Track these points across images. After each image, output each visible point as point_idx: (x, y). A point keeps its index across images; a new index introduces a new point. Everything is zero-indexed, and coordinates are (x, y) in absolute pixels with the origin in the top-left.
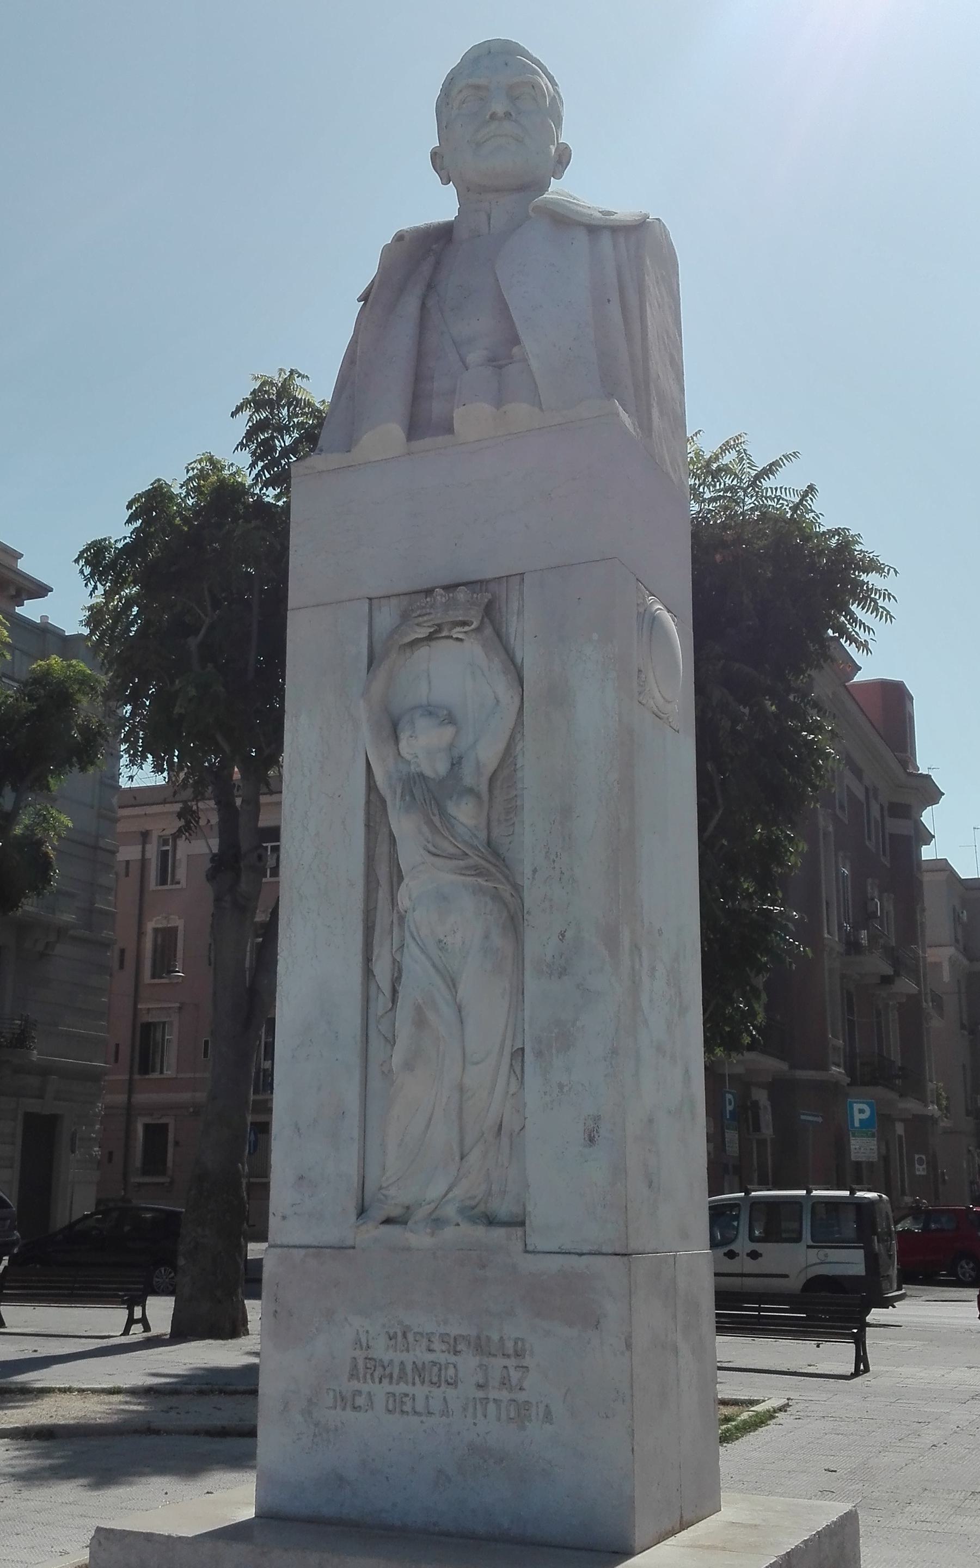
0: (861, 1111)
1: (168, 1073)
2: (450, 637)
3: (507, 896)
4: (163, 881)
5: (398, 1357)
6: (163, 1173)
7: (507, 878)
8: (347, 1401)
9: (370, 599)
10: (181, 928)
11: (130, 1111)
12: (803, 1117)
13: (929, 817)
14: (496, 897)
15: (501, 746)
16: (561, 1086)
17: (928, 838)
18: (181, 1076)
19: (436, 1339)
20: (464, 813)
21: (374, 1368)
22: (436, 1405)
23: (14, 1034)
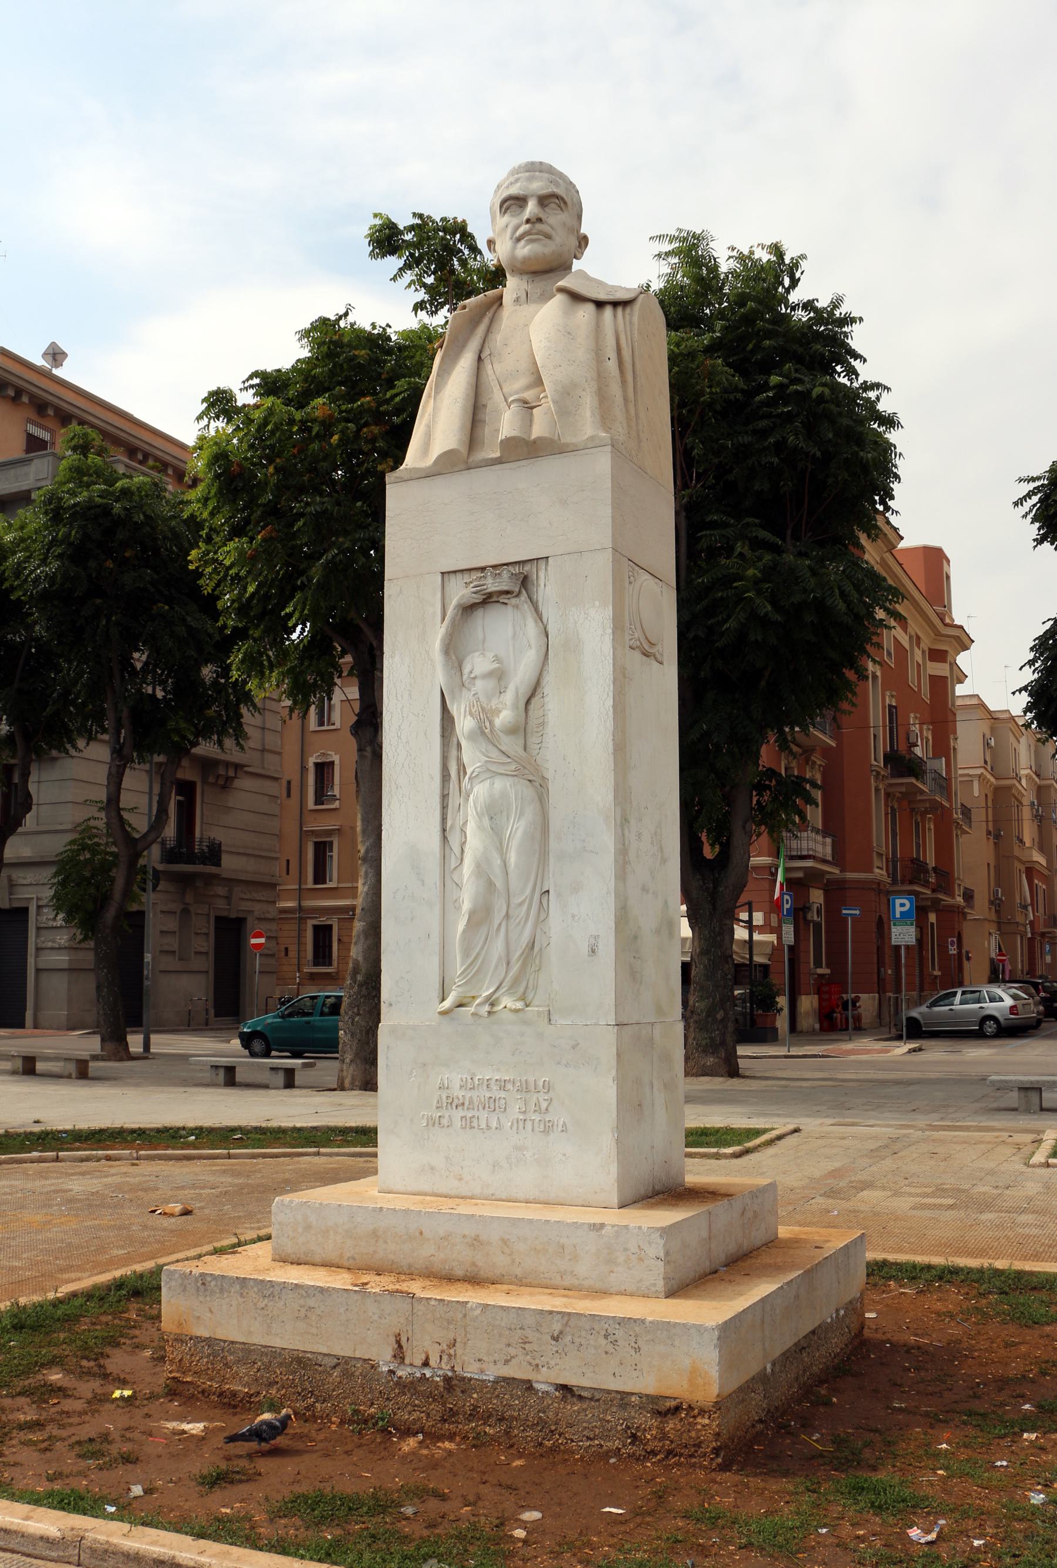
0: (903, 905)
10: (337, 762)
12: (844, 912)
13: (963, 660)
16: (573, 916)
17: (962, 678)
18: (341, 885)
19: (492, 1082)
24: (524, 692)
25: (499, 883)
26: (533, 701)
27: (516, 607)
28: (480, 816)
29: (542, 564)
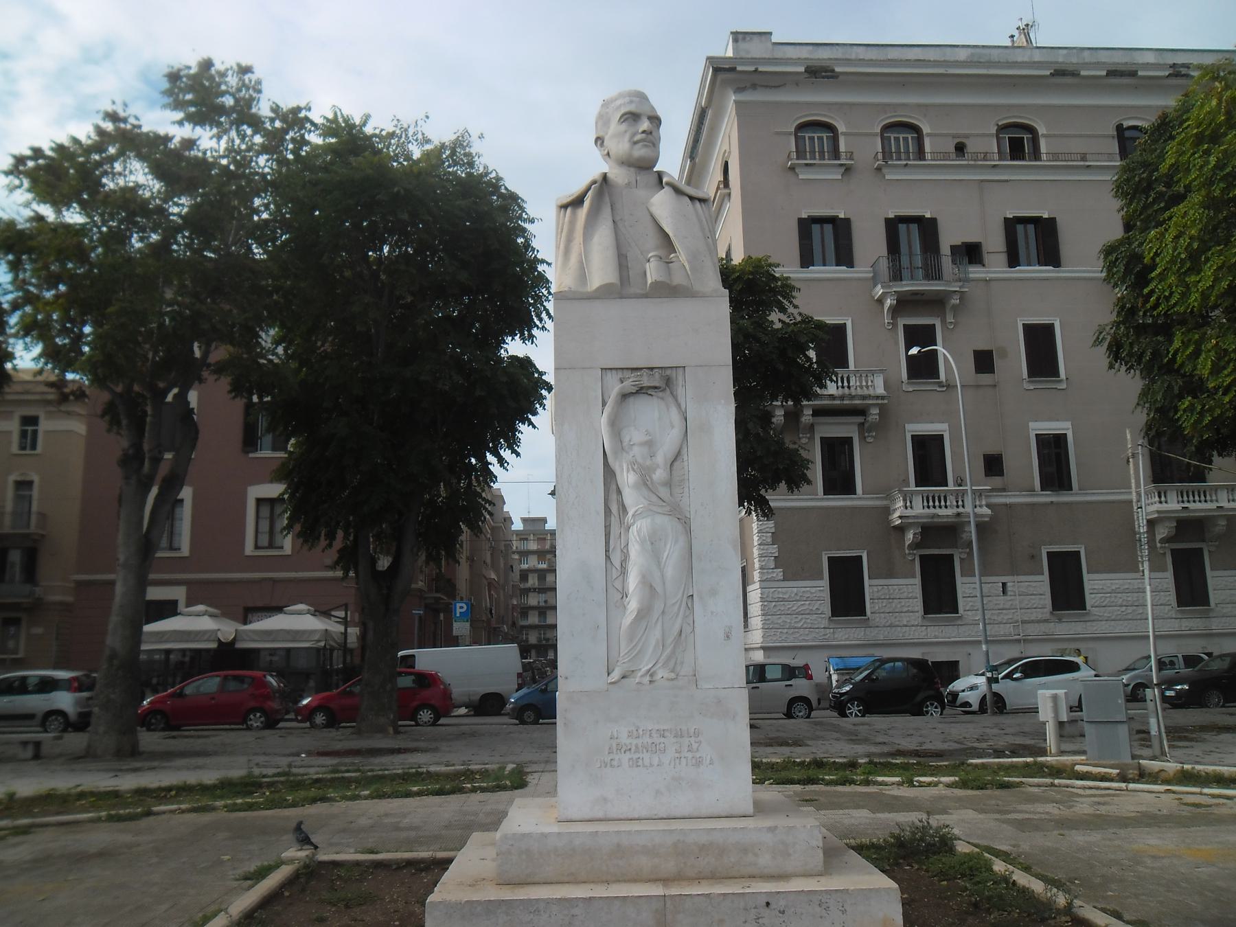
24: (671, 456)
25: (659, 589)
26: (676, 464)
27: (662, 398)
28: (642, 542)
29: (680, 371)
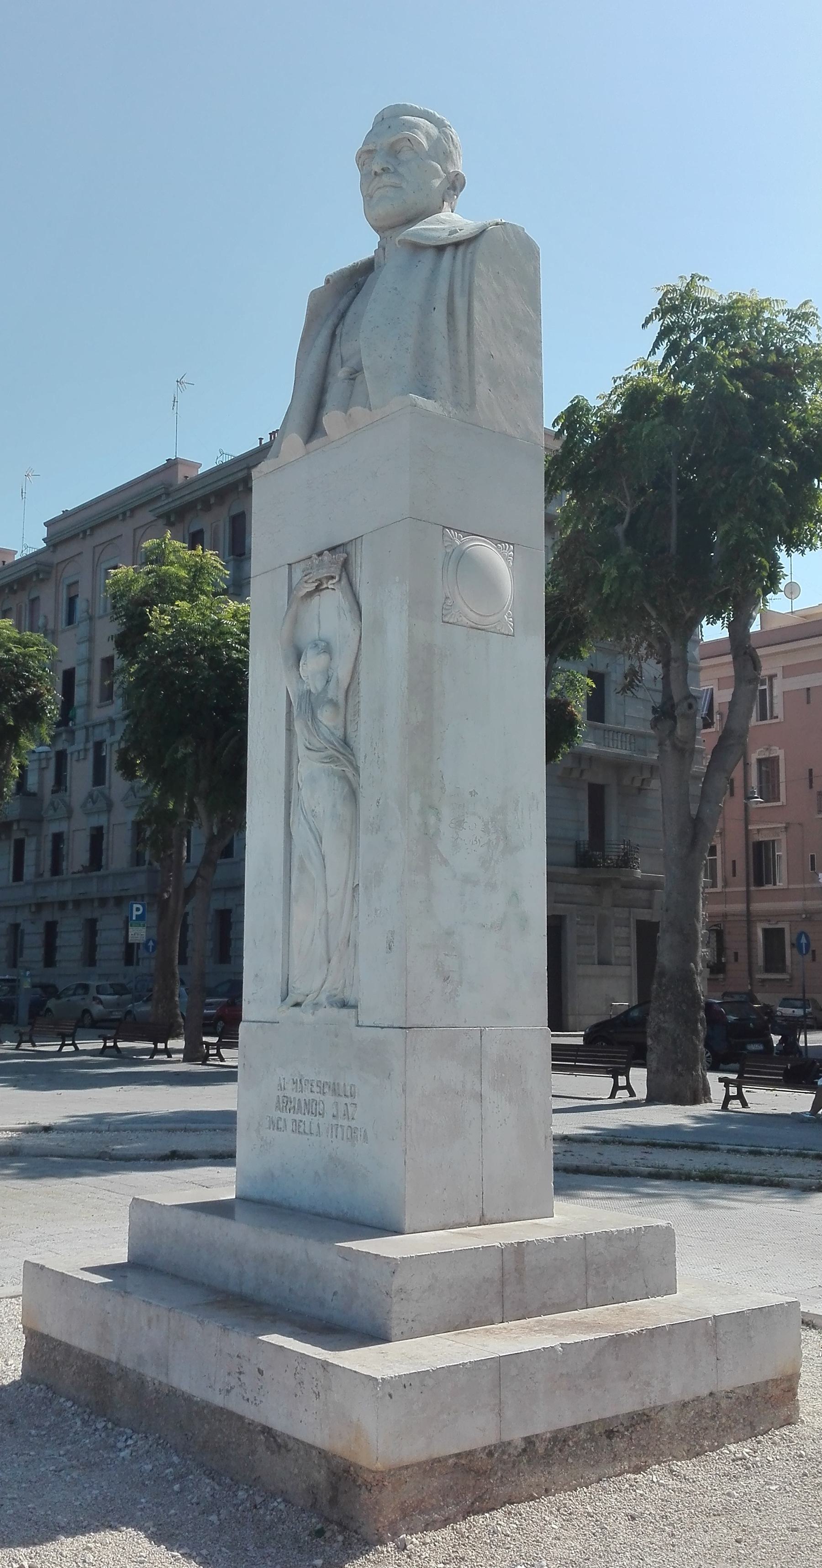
1: (780, 885)
2: (328, 588)
3: (350, 775)
4: (763, 717)
5: (298, 1096)
6: (783, 970)
7: (351, 763)
8: (275, 1125)
9: (290, 565)
10: (782, 758)
11: (749, 918)
14: (344, 778)
15: (350, 666)
18: (791, 887)
20: (325, 716)
21: (285, 1103)
22: (314, 1129)
23: (619, 856)
